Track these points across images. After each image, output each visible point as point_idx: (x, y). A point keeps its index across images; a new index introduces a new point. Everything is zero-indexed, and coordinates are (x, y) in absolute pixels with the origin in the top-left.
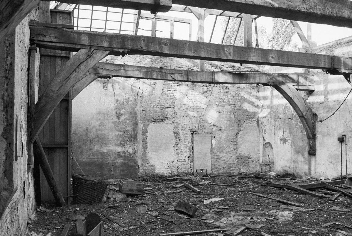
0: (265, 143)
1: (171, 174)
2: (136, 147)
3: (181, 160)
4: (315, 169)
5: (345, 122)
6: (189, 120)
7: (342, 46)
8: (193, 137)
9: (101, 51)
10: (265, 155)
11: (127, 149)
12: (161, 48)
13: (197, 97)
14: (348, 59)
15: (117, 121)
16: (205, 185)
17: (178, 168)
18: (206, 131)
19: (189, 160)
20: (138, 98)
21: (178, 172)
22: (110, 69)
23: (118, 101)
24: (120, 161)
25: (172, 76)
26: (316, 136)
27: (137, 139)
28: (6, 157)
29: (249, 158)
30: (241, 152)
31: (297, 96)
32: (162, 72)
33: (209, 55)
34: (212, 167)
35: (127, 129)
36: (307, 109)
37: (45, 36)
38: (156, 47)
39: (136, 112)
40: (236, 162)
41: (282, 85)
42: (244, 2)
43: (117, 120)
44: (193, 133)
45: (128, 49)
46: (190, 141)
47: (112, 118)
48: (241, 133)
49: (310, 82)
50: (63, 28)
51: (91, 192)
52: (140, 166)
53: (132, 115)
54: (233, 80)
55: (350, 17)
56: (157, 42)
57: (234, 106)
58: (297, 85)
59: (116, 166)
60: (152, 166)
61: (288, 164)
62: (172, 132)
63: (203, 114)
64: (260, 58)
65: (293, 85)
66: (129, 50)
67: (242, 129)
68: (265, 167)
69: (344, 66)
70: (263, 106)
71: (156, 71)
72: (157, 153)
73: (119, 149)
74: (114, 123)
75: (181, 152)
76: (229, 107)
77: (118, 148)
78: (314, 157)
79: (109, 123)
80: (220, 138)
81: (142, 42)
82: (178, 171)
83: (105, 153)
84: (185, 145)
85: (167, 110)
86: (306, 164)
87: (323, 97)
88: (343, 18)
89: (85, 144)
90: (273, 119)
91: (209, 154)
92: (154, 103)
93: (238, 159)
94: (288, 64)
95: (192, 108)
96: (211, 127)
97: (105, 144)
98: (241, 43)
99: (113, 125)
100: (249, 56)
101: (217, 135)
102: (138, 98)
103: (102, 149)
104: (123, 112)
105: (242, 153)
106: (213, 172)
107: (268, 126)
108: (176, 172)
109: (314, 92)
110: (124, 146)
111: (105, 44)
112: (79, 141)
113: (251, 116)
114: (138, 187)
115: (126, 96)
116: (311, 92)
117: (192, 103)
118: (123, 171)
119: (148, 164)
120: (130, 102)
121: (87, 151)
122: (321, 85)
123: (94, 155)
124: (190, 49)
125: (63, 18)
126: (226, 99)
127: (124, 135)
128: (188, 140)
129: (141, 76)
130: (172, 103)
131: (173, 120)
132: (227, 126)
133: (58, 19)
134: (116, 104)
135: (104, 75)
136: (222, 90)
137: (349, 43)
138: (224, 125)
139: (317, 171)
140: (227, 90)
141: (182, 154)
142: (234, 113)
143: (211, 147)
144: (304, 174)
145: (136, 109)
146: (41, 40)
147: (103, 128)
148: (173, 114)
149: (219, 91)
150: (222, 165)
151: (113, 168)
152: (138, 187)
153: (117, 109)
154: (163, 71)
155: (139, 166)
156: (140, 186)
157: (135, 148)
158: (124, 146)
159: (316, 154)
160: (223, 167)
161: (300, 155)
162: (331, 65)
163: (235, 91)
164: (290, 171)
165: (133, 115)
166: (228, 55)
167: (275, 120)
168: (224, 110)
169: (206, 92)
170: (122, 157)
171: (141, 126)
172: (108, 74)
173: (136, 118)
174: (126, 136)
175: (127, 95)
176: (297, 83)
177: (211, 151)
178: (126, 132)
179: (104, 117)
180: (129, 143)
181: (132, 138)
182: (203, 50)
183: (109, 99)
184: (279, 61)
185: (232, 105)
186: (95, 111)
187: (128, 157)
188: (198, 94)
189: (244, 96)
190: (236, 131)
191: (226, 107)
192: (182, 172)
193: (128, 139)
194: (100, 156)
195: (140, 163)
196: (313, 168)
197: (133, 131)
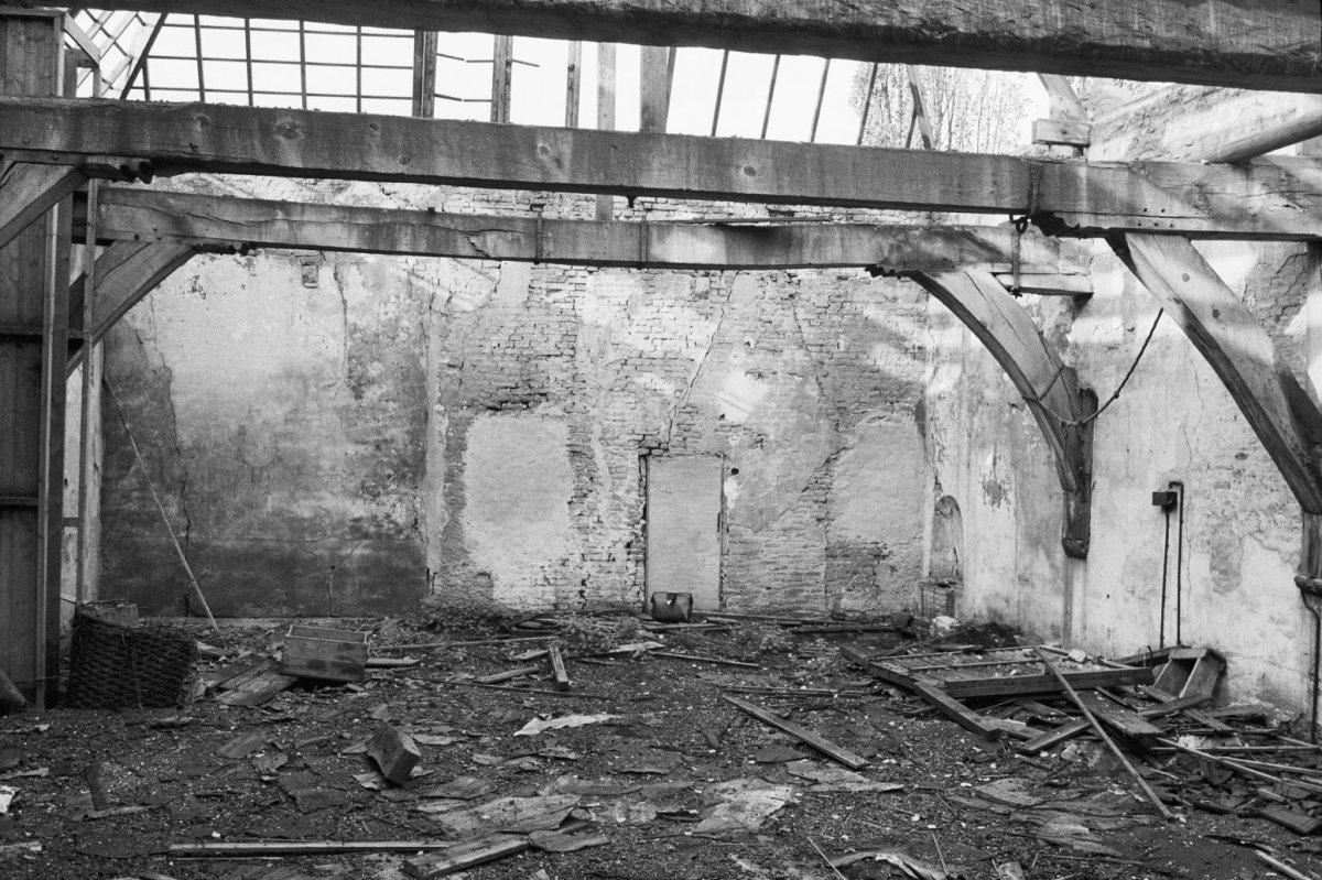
0: (938, 499)
1: (556, 605)
2: (422, 503)
3: (596, 557)
4: (1084, 615)
5: (1183, 427)
6: (632, 405)
7: (1183, 111)
8: (647, 469)
9: (42, 166)
10: (942, 547)
11: (387, 509)
12: (273, 148)
13: (667, 317)
14: (1111, 171)
15: (353, 403)
16: (635, 656)
17: (583, 583)
18: (702, 445)
19: (631, 556)
20: (434, 318)
21: (582, 600)
22: (235, 220)
23: (355, 329)
24: (359, 551)
25: (473, 240)
26: (1090, 479)
27: (424, 473)
29: (877, 556)
30: (843, 532)
31: (1010, 317)
32: (434, 228)
33: (469, 165)
34: (721, 587)
35: (388, 436)
36: (1053, 369)
38: (253, 145)
39: (422, 373)
40: (822, 569)
41: (944, 275)
44: (649, 452)
46: (635, 485)
47: (332, 394)
48: (844, 456)
49: (1069, 258)
52: (435, 573)
53: (407, 384)
54: (729, 251)
55: (773, 14)
57: (821, 352)
58: (1011, 273)
60: (482, 574)
61: (1004, 588)
62: (564, 450)
63: (690, 381)
64: (694, 177)
65: (995, 274)
66: (147, 161)
67: (851, 440)
68: (932, 594)
69: (1089, 198)
70: (937, 353)
71: (413, 225)
72: (502, 528)
73: (359, 509)
74: (343, 412)
75: (595, 525)
76: (800, 355)
77: (354, 504)
78: (1082, 563)
79: (321, 410)
80: (759, 474)
81: (198, 127)
82: (582, 596)
84: (615, 497)
85: (543, 364)
86: (1056, 591)
87: (1117, 322)
88: (740, 18)
89: (233, 488)
90: (965, 405)
91: (711, 535)
92: (495, 340)
93: (831, 559)
94: (821, 196)
95: (644, 356)
96: (721, 433)
97: (307, 489)
98: (628, 120)
99: (335, 418)
100: (641, 166)
101: (744, 462)
102: (434, 318)
103: (294, 507)
104: (374, 370)
105: (851, 536)
106: (724, 605)
107: (949, 430)
108: (574, 599)
109: (1090, 302)
110: (376, 496)
111: (55, 142)
113: (892, 393)
114: (345, 654)
115: (386, 313)
116: (1080, 301)
117: (647, 338)
118: (372, 588)
119: (464, 565)
120: (403, 336)
121: (239, 513)
122: (1114, 272)
123: (264, 526)
124: (387, 148)
125: (28, 39)
126: (788, 324)
127: (376, 456)
128: (626, 482)
129: (353, 245)
130: (567, 338)
131: (569, 401)
132: (786, 430)
133: (9, 44)
134: (349, 343)
135: (211, 242)
136: (771, 289)
137: (1207, 97)
138: (775, 425)
139: (1090, 621)
140: (790, 290)
141: (603, 532)
142: (822, 380)
143: (719, 510)
144: (1048, 632)
145: (423, 361)
148: (570, 381)
149: (760, 292)
150: (765, 580)
151: (332, 576)
152: (345, 654)
153: (354, 361)
154: (437, 222)
155: (431, 574)
157: (418, 506)
158: (376, 496)
159: (1089, 556)
160: (768, 588)
161: (1042, 556)
162: (1030, 196)
163: (829, 290)
164: (1010, 615)
165: (414, 384)
166: (552, 166)
167: (972, 411)
168: (778, 366)
169: (705, 295)
170: (366, 536)
171: (440, 424)
173: (424, 395)
174: (385, 460)
175: (391, 308)
176: (1010, 266)
177: (720, 524)
178: (383, 447)
180: (393, 487)
181: (406, 469)
182: (444, 148)
184: (780, 187)
185: (814, 349)
186: (273, 367)
187: (389, 537)
188: (669, 302)
189: (866, 313)
190: (827, 450)
191: (786, 355)
192: (599, 602)
193: (391, 472)
194: (286, 534)
195: (433, 561)
196: (1077, 611)
197: (411, 442)
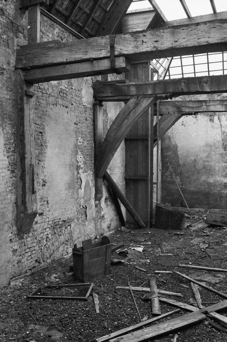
12: (202, 87)
15: (224, 152)
28: (23, 192)
37: (104, 92)
38: (197, 87)
42: (197, 45)
43: (224, 151)
45: (170, 93)
50: (117, 83)
51: (167, 219)
56: (198, 82)
59: (222, 197)
66: (171, 94)
81: (183, 84)
83: (212, 183)
97: (212, 175)
103: (209, 180)
111: (150, 92)
112: (188, 172)
114: (223, 219)
121: (195, 181)
123: (201, 185)
125: (142, 68)
134: (223, 136)
135: (187, 112)
146: (101, 96)
147: (209, 159)
152: (223, 219)
156: (225, 218)
172: (190, 111)
179: (211, 149)
183: (215, 131)
186: (202, 143)
194: (206, 186)
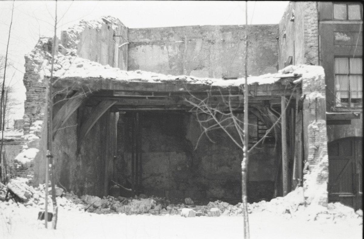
23: (170, 57)
47: (166, 68)
104: (174, 63)
120: (179, 57)
175: (176, 53)
